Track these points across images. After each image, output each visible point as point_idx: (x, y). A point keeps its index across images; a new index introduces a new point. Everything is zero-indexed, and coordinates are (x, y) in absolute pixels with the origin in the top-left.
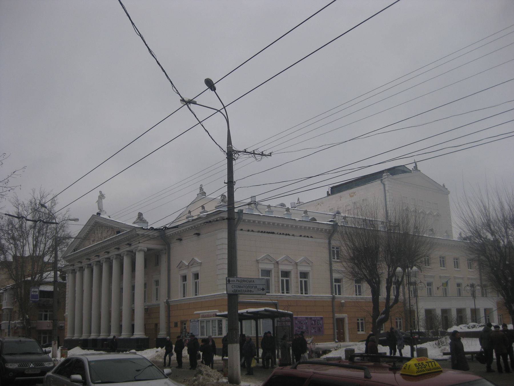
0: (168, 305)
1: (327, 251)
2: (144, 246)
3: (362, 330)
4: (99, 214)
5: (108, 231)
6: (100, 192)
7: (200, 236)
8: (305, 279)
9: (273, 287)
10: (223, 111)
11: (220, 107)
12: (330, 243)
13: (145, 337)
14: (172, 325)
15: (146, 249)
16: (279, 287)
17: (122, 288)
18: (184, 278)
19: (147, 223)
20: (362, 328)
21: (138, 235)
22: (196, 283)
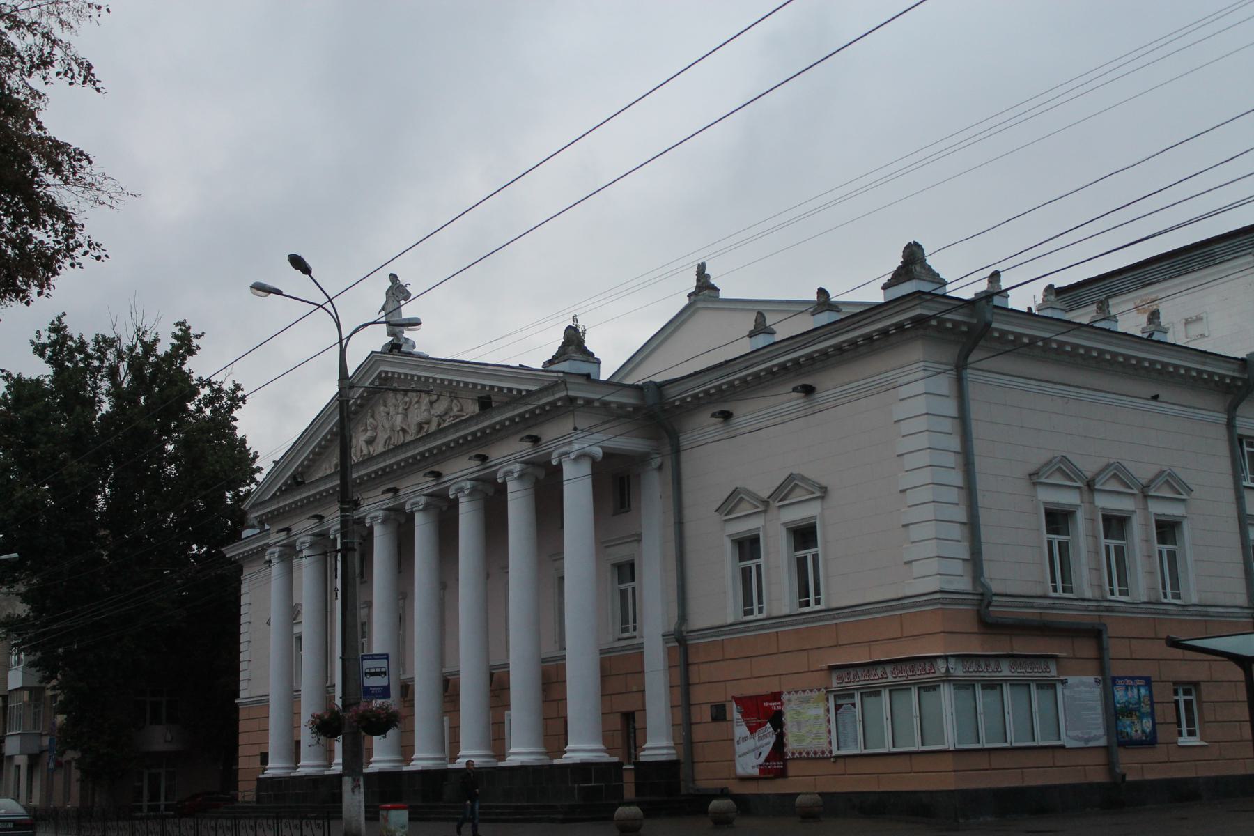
0: (681, 643)
1: (1223, 449)
2: (594, 442)
3: (1191, 733)
4: (394, 347)
5: (431, 403)
6: (393, 277)
7: (817, 396)
8: (1171, 547)
9: (1085, 572)
10: (329, 306)
11: (322, 299)
12: (1230, 425)
13: (606, 758)
14: (705, 714)
15: (598, 452)
16: (1098, 570)
17: (562, 578)
18: (748, 546)
19: (598, 362)
20: (1190, 722)
21: (571, 400)
22: (802, 562)
